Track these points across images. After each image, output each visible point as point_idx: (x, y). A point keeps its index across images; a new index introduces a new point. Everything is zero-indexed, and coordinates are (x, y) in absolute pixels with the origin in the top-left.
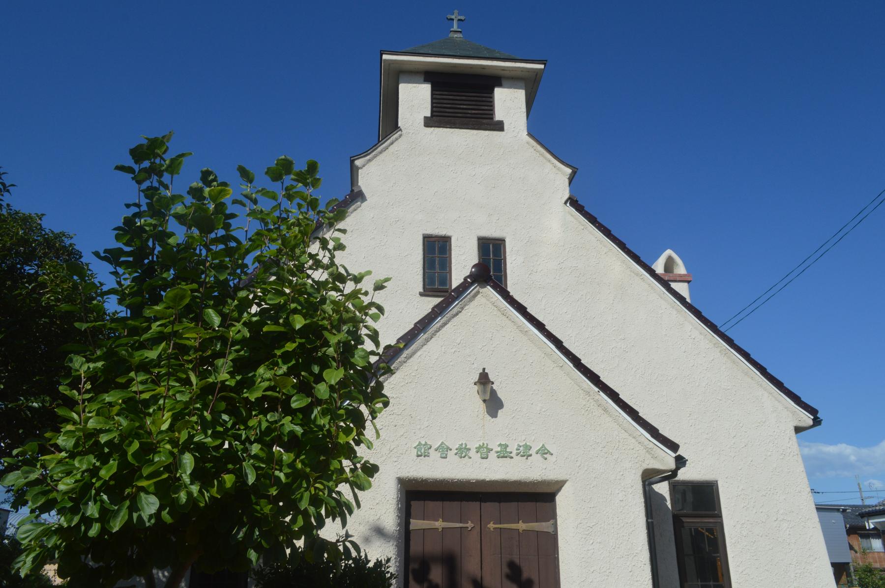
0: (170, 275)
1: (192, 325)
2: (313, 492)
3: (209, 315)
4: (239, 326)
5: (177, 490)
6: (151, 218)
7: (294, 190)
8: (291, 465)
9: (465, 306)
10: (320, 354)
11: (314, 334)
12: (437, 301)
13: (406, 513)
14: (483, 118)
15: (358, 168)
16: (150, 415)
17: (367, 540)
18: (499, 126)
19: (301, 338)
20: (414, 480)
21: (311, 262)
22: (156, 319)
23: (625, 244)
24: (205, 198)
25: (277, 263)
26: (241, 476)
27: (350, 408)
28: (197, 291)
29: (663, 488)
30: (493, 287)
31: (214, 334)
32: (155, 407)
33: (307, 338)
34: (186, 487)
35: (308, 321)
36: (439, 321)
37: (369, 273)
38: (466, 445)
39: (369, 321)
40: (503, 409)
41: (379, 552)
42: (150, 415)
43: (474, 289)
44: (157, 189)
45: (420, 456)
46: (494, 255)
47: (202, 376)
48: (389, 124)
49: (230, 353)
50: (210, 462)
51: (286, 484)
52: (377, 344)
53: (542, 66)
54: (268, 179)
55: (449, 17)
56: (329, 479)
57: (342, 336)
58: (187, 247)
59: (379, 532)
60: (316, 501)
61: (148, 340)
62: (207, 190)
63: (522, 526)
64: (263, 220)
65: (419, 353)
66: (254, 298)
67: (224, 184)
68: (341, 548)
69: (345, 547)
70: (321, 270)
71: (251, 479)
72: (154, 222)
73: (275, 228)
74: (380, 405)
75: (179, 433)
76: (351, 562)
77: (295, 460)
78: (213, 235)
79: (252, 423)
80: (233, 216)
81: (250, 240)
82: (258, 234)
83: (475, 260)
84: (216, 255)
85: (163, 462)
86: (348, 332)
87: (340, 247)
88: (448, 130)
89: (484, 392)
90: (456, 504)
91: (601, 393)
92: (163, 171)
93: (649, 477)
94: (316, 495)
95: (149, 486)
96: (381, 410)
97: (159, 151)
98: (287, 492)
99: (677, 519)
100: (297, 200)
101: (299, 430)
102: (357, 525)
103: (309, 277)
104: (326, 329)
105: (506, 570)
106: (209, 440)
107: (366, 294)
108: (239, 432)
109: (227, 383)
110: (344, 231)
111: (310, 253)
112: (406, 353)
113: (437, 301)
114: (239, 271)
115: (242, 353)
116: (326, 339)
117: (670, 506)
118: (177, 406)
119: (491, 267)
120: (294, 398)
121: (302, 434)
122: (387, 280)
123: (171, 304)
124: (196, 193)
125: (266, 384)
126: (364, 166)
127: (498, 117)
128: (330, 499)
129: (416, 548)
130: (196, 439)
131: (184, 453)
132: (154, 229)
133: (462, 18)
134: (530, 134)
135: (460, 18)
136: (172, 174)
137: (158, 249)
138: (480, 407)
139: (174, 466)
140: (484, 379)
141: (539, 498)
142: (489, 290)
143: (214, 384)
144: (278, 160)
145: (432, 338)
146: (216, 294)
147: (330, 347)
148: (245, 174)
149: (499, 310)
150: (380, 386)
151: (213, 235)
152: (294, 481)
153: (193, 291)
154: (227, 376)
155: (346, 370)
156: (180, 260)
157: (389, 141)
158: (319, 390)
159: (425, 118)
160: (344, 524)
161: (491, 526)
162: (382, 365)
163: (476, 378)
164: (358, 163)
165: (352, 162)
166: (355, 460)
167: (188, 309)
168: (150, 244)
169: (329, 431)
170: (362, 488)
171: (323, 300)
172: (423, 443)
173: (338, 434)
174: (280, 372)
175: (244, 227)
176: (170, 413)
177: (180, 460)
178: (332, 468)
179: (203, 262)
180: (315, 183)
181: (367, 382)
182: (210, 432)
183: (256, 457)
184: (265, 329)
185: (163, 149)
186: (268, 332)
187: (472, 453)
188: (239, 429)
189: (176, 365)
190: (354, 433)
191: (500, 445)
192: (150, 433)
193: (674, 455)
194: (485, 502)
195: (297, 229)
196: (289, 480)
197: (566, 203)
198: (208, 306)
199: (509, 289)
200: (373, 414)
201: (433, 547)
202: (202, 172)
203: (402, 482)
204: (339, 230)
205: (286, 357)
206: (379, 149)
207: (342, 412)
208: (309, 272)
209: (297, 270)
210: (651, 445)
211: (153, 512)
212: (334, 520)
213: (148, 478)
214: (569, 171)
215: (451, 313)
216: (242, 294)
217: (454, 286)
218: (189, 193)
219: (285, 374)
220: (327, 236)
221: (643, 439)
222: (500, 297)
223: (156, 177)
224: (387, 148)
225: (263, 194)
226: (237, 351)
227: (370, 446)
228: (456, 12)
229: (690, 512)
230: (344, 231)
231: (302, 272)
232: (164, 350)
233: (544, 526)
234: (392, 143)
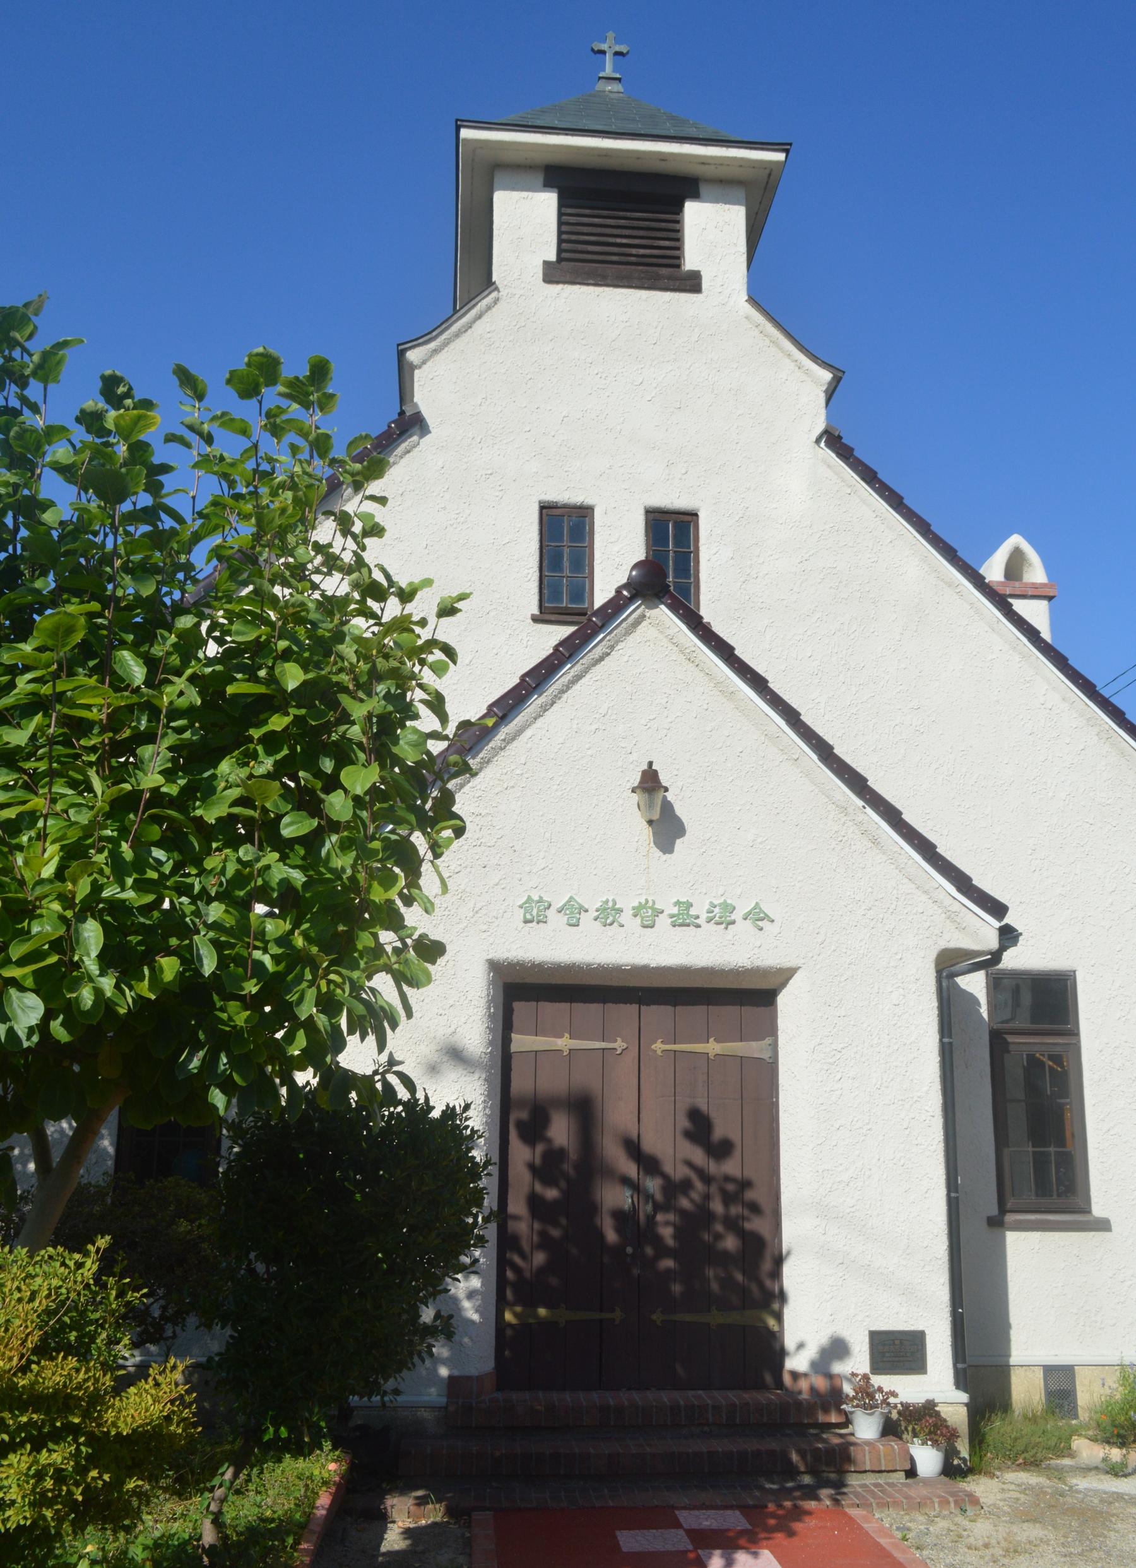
0: (47, 583)
1: (92, 681)
2: (324, 989)
3: (122, 662)
4: (180, 683)
5: (76, 984)
6: (9, 470)
7: (284, 417)
8: (284, 941)
9: (617, 642)
10: (334, 737)
11: (321, 695)
12: (564, 631)
13: (504, 1024)
14: (657, 264)
15: (413, 367)
16: (20, 848)
17: (433, 1069)
18: (692, 283)
19: (298, 707)
20: (518, 963)
21: (319, 559)
22: (27, 669)
23: (929, 525)
24: (109, 433)
25: (253, 560)
26: (189, 959)
27: (394, 837)
28: (101, 615)
29: (975, 984)
30: (670, 607)
31: (135, 699)
32: (33, 833)
33: (310, 706)
34: (91, 980)
35: (310, 676)
36: (567, 672)
37: (428, 582)
38: (615, 903)
39: (427, 676)
41: (458, 1093)
42: (20, 848)
43: (635, 609)
44: (16, 413)
45: (531, 921)
46: (676, 544)
47: (116, 776)
48: (474, 272)
49: (165, 735)
50: (136, 933)
51: (275, 973)
52: (443, 718)
53: (780, 157)
54: (231, 393)
55: (598, 46)
56: (354, 966)
57: (375, 704)
58: (77, 529)
59: (456, 1055)
60: (329, 1005)
61: (14, 707)
62: (112, 414)
63: (713, 1047)
64: (225, 476)
65: (528, 733)
66: (210, 630)
67: (147, 404)
68: (379, 1086)
69: (387, 1086)
70: (337, 576)
71: (209, 966)
72: (13, 479)
73: (250, 493)
74: (448, 833)
75: (74, 882)
76: (400, 1108)
77: (291, 932)
78: (126, 507)
79: (210, 863)
80: (165, 469)
81: (200, 514)
82: (215, 504)
83: (640, 555)
84: (132, 545)
85: (47, 934)
86: (388, 697)
87: (375, 530)
88: (591, 289)
89: (650, 805)
90: (595, 1008)
91: (869, 810)
92: (28, 376)
93: (949, 965)
94: (330, 994)
95: (24, 976)
96: (449, 841)
97: (18, 336)
98: (275, 987)
99: (998, 1040)
100: (291, 437)
101: (298, 877)
102: (410, 1046)
103: (315, 587)
104: (345, 690)
105: (684, 1123)
106: (130, 894)
107: (423, 623)
108: (189, 880)
109: (164, 789)
110: (382, 500)
111: (316, 543)
112: (504, 732)
113: (564, 631)
114: (180, 576)
115: (187, 735)
116: (344, 709)
117: (985, 1015)
118: (70, 833)
119: (669, 565)
120: (286, 820)
121: (305, 885)
122: (462, 597)
123: (50, 643)
124: (91, 420)
125: (235, 793)
126: (424, 362)
127: (690, 262)
128: (356, 1003)
129: (521, 1084)
130: (105, 894)
131: (84, 921)
132: (15, 492)
133: (623, 48)
134: (752, 300)
135: (618, 48)
136: (45, 381)
137: (24, 533)
139: (65, 945)
140: (650, 782)
141: (748, 998)
142: (663, 613)
143: (136, 794)
144: (250, 356)
145: (553, 703)
146: (138, 619)
147: (353, 723)
148: (186, 378)
150: (447, 799)
151: (126, 507)
152: (289, 969)
153: (91, 615)
154: (160, 780)
155: (382, 767)
156: (67, 553)
157: (473, 313)
158: (331, 804)
159: (547, 264)
160: (381, 1045)
161: (659, 1046)
162: (453, 758)
163: (636, 779)
164: (413, 356)
165: (401, 354)
166: (403, 933)
167: (86, 650)
168: (9, 520)
169: (353, 879)
170: (414, 983)
171: (339, 636)
172: (536, 898)
173: (370, 886)
174: (261, 770)
175: (189, 489)
176: (57, 847)
177: (77, 931)
178: (360, 947)
179: (107, 559)
180: (325, 403)
181: (423, 789)
182: (129, 881)
183: (216, 926)
184: (230, 690)
185: (28, 332)
186: (236, 696)
187: (626, 917)
188: (189, 875)
189: (67, 756)
190: (402, 882)
191: (678, 903)
192: (22, 883)
193: (997, 924)
194: (648, 1005)
195: (289, 494)
196: (281, 968)
197: (818, 441)
198: (123, 644)
199: (702, 613)
200: (436, 850)
201: (552, 1082)
202: (103, 378)
203: (496, 967)
204: (372, 498)
205: (271, 742)
206: (455, 328)
207: (376, 845)
208: (316, 578)
209: (292, 576)
210: (956, 907)
211: (34, 1022)
212: (363, 1039)
213: (22, 962)
214: (827, 376)
215: (591, 656)
216: (185, 622)
217: (597, 604)
218: (78, 420)
219: (269, 776)
220: (350, 508)
221: (942, 895)
222: (684, 627)
223: (14, 388)
224: (469, 326)
225: (223, 425)
226: (179, 731)
227: (428, 909)
228: (611, 35)
229: (1027, 1025)
230: (382, 500)
231: (303, 578)
232: (40, 729)
233: (754, 1049)
234: (479, 317)
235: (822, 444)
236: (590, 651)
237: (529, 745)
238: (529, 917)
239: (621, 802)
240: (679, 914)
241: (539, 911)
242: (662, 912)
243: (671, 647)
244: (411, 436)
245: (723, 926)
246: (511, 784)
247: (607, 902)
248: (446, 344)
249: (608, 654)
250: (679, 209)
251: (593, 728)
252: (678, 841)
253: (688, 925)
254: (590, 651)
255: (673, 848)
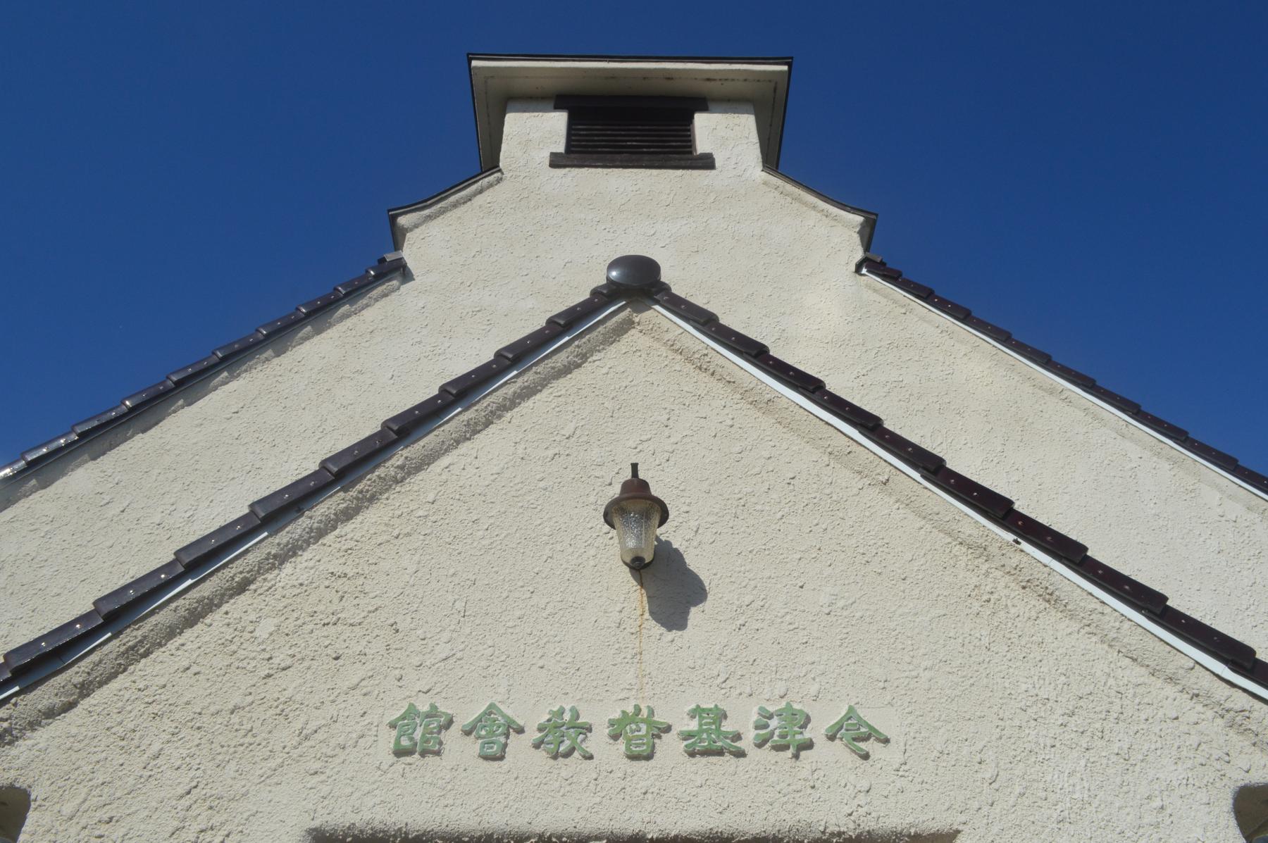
9: (592, 351)
15: (404, 231)
38: (576, 715)
40: (708, 605)
43: (617, 313)
53: (785, 68)
65: (445, 461)
91: (1025, 546)
126: (416, 226)
138: (629, 595)
140: (637, 503)
145: (488, 424)
149: (689, 360)
157: (474, 187)
159: (553, 155)
164: (403, 221)
165: (393, 219)
172: (424, 708)
187: (597, 742)
191: (696, 712)
206: (453, 199)
210: (1242, 700)
215: (550, 363)
234: (481, 191)
235: (864, 271)
236: (547, 357)
237: (444, 477)
238: (405, 742)
239: (592, 552)
240: (701, 731)
241: (428, 731)
242: (668, 729)
243: (671, 355)
244: (390, 280)
245: (789, 753)
246: (408, 530)
247: (561, 712)
248: (443, 212)
249: (579, 366)
250: (690, 120)
251: (550, 453)
252: (693, 610)
253: (720, 753)
254: (547, 357)
255: (686, 620)
